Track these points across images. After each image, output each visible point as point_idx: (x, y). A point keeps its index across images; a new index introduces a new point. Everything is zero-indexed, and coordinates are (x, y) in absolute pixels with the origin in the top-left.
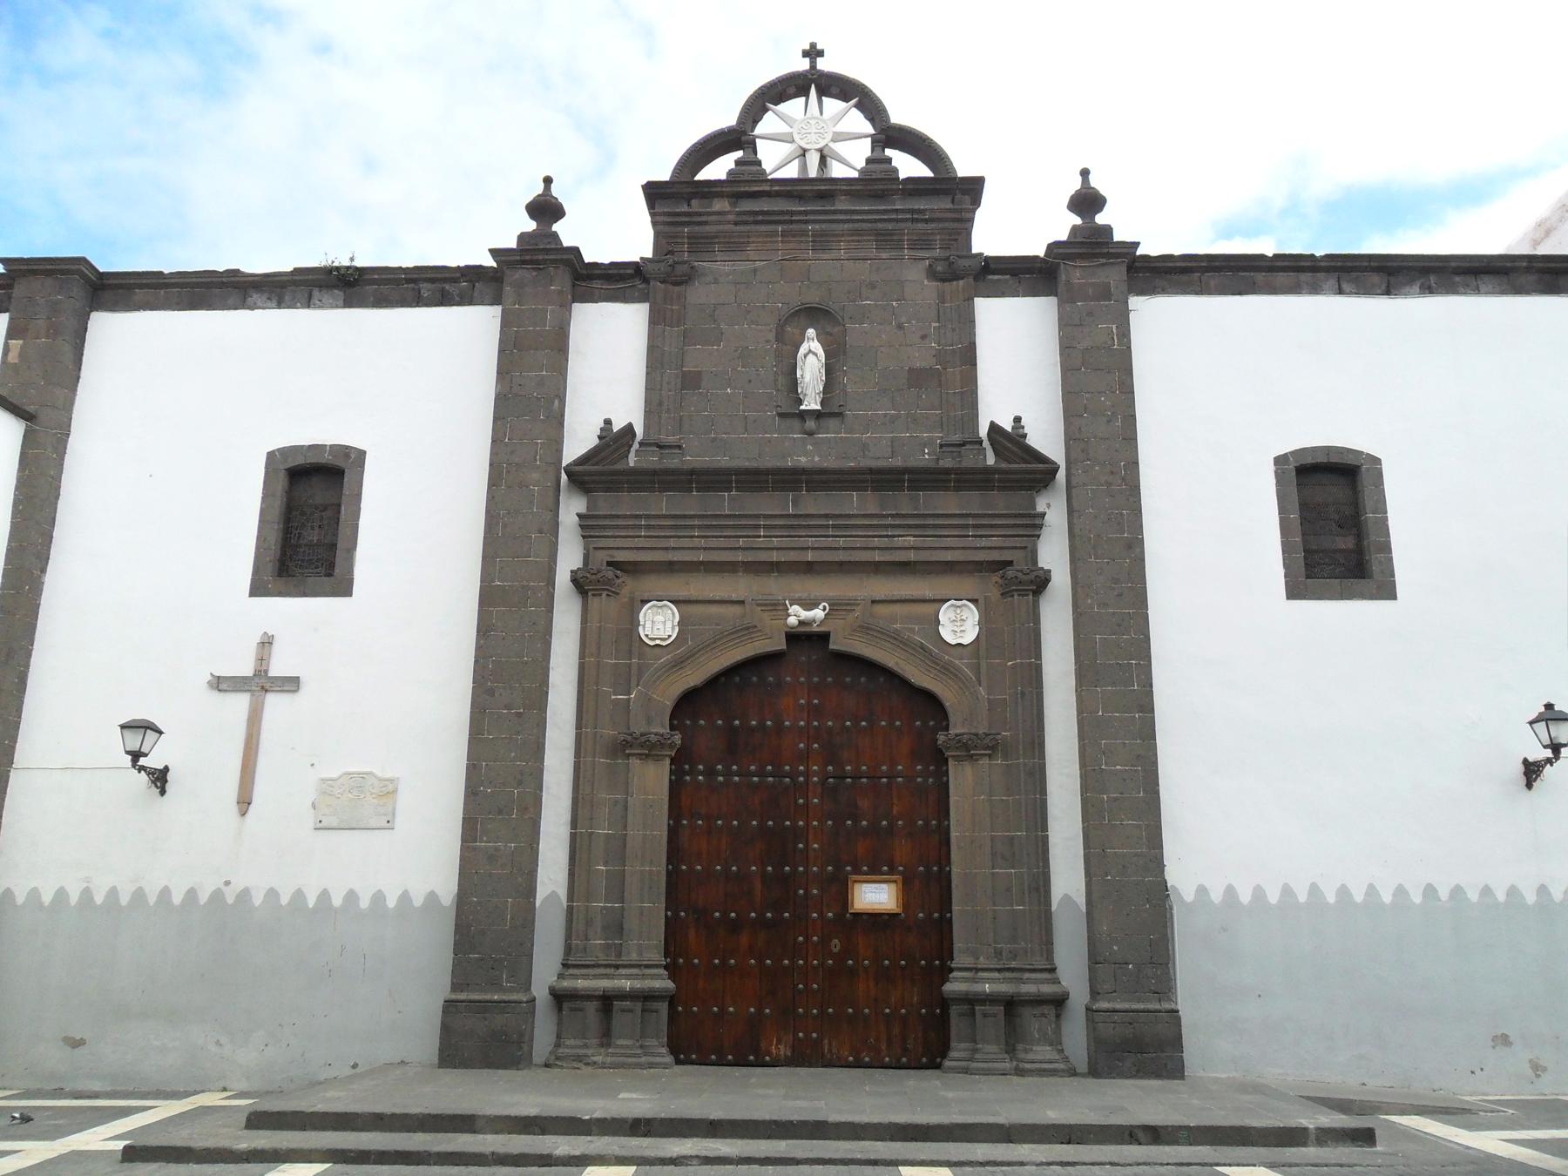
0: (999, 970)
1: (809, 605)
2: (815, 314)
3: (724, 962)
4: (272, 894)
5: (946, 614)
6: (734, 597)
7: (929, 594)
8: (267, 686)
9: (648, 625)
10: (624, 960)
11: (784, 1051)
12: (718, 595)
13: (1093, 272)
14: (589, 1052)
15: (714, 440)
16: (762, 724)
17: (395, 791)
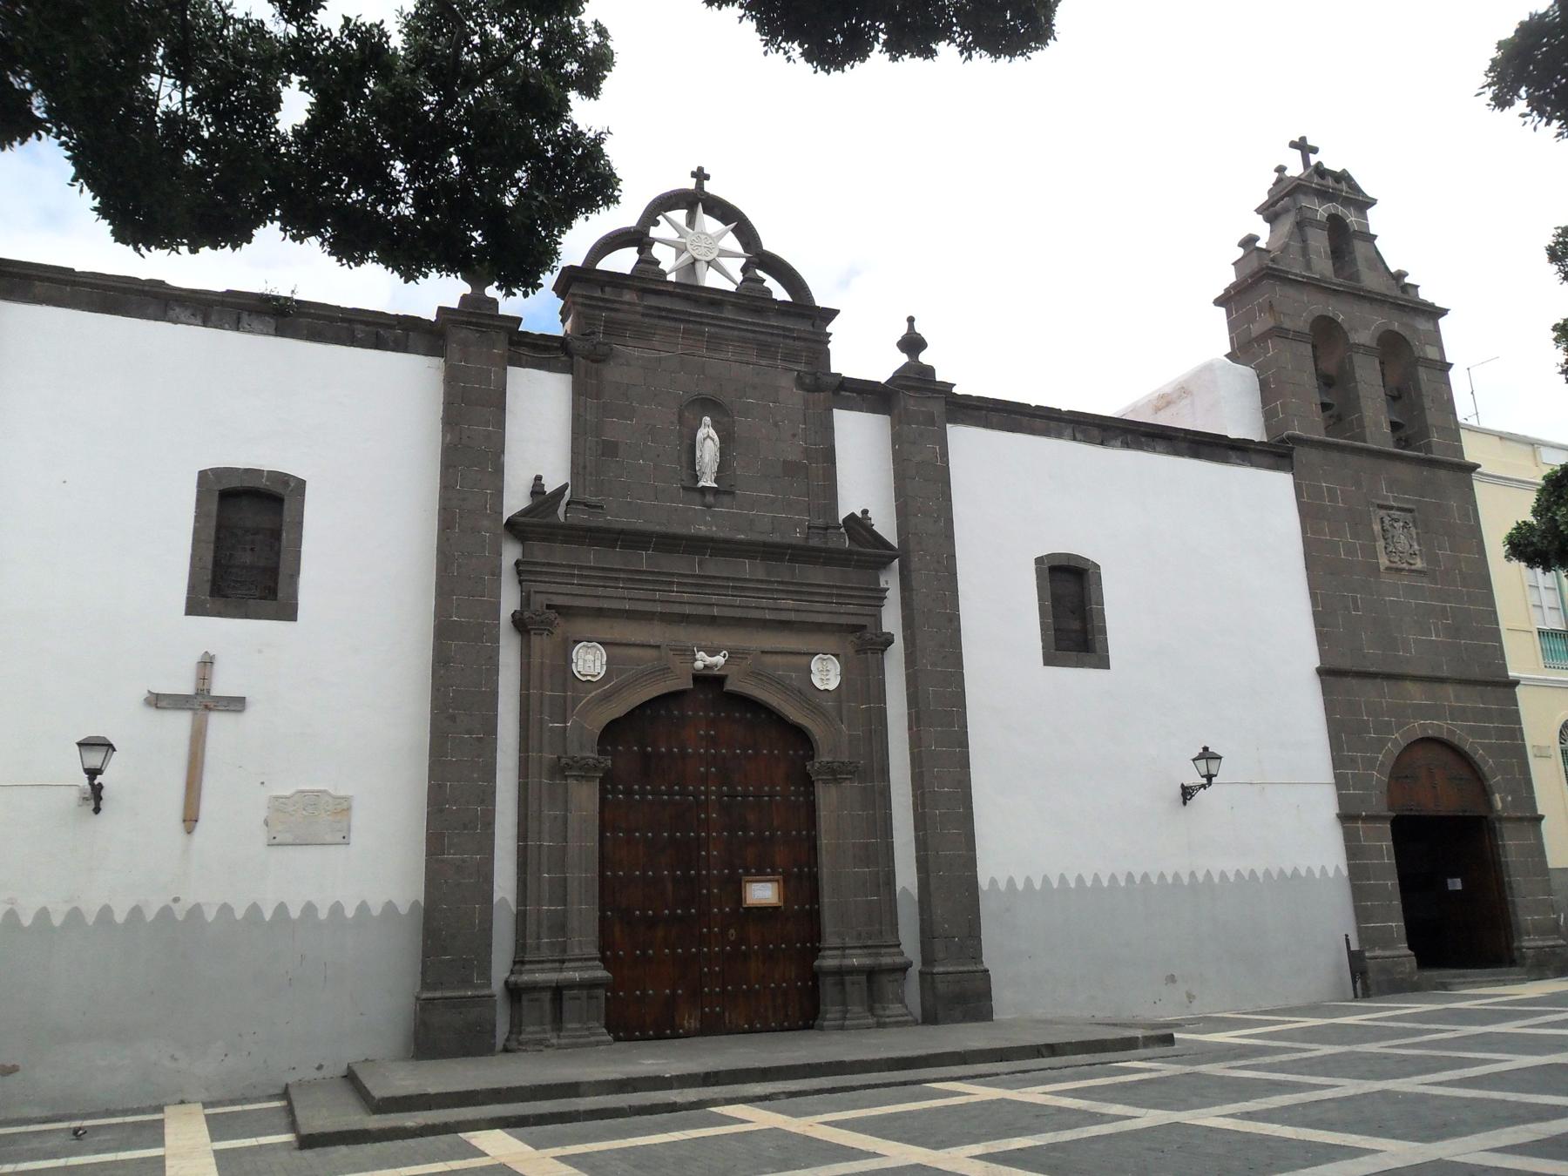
1: (712, 652)
2: (709, 404)
3: (644, 953)
4: (225, 909)
5: (815, 664)
7: (804, 649)
8: (211, 705)
9: (580, 662)
11: (691, 1023)
13: (919, 403)
16: (670, 750)
17: (349, 809)
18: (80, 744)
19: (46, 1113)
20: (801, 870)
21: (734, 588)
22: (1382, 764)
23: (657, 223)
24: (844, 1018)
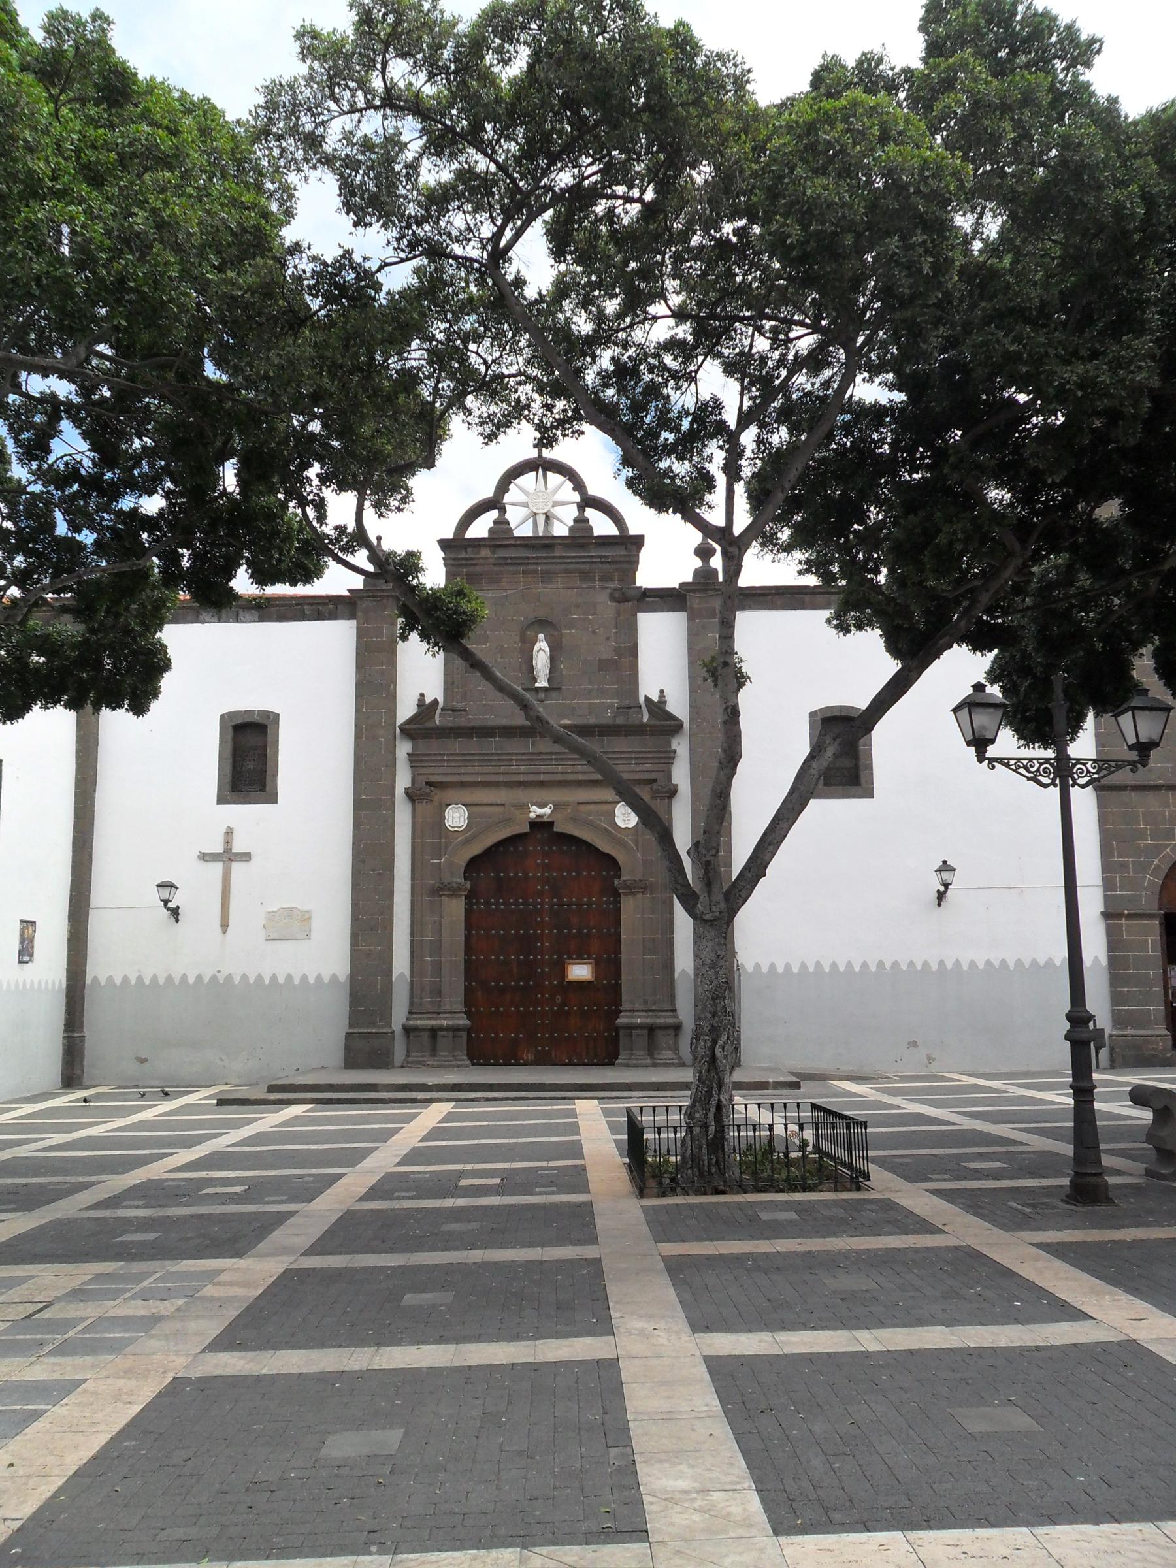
1: (541, 806)
2: (543, 624)
4: (245, 977)
6: (499, 801)
12: (486, 800)
16: (516, 875)
17: (310, 918)
22: (1158, 867)
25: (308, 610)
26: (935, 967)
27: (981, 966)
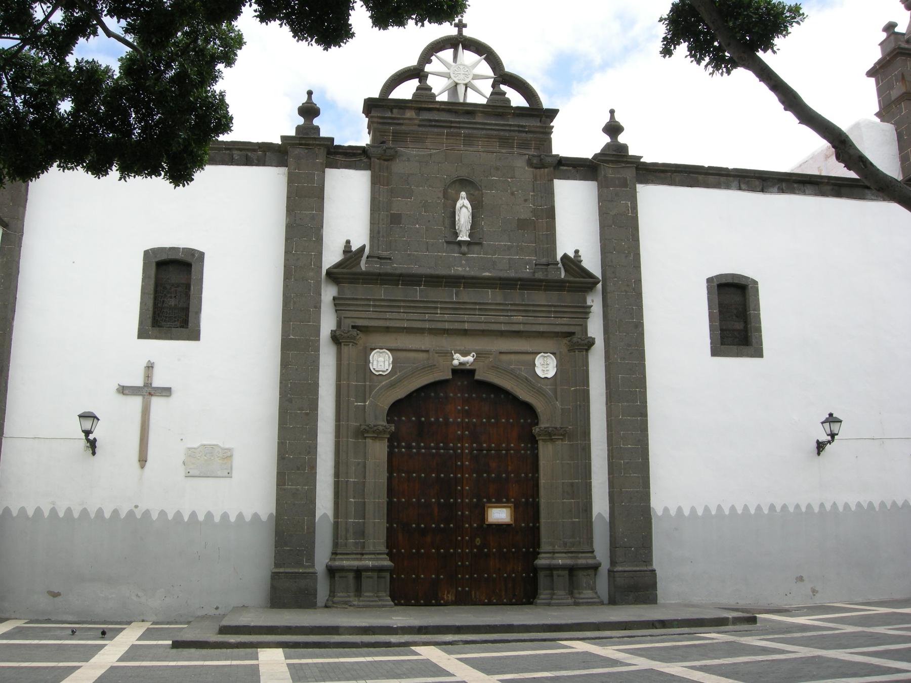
0: (565, 553)
1: (465, 354)
2: (464, 183)
4: (163, 513)
5: (539, 360)
6: (423, 348)
7: (530, 350)
8: (152, 392)
9: (375, 363)
10: (366, 550)
12: (414, 347)
13: (617, 171)
14: (351, 599)
15: (409, 255)
17: (231, 456)
18: (80, 416)
19: (76, 619)
20: (527, 500)
21: (480, 309)
23: (430, 62)
24: (551, 599)
25: (236, 154)
26: (816, 509)
27: (853, 508)
